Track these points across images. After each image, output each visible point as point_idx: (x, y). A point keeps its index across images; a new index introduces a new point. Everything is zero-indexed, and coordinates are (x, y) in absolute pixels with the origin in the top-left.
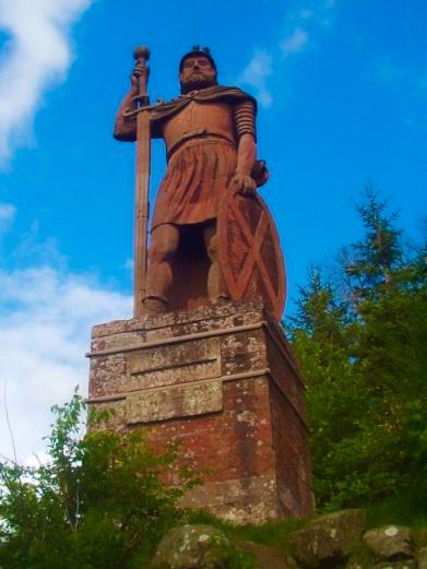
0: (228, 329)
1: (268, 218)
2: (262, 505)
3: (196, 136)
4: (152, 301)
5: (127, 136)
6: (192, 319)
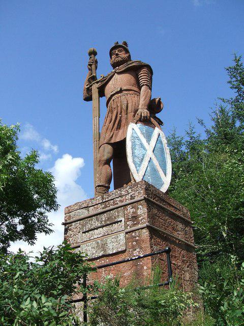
5: (89, 98)
6: (110, 198)
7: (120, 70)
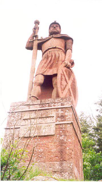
0: (59, 107)
1: (74, 76)
2: (67, 173)
3: (53, 48)
4: (33, 98)
6: (46, 103)
7: (57, 37)
